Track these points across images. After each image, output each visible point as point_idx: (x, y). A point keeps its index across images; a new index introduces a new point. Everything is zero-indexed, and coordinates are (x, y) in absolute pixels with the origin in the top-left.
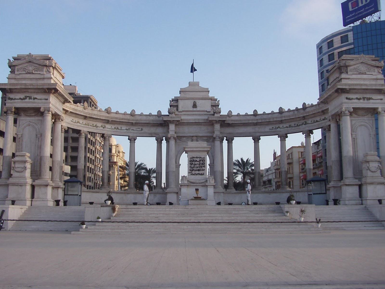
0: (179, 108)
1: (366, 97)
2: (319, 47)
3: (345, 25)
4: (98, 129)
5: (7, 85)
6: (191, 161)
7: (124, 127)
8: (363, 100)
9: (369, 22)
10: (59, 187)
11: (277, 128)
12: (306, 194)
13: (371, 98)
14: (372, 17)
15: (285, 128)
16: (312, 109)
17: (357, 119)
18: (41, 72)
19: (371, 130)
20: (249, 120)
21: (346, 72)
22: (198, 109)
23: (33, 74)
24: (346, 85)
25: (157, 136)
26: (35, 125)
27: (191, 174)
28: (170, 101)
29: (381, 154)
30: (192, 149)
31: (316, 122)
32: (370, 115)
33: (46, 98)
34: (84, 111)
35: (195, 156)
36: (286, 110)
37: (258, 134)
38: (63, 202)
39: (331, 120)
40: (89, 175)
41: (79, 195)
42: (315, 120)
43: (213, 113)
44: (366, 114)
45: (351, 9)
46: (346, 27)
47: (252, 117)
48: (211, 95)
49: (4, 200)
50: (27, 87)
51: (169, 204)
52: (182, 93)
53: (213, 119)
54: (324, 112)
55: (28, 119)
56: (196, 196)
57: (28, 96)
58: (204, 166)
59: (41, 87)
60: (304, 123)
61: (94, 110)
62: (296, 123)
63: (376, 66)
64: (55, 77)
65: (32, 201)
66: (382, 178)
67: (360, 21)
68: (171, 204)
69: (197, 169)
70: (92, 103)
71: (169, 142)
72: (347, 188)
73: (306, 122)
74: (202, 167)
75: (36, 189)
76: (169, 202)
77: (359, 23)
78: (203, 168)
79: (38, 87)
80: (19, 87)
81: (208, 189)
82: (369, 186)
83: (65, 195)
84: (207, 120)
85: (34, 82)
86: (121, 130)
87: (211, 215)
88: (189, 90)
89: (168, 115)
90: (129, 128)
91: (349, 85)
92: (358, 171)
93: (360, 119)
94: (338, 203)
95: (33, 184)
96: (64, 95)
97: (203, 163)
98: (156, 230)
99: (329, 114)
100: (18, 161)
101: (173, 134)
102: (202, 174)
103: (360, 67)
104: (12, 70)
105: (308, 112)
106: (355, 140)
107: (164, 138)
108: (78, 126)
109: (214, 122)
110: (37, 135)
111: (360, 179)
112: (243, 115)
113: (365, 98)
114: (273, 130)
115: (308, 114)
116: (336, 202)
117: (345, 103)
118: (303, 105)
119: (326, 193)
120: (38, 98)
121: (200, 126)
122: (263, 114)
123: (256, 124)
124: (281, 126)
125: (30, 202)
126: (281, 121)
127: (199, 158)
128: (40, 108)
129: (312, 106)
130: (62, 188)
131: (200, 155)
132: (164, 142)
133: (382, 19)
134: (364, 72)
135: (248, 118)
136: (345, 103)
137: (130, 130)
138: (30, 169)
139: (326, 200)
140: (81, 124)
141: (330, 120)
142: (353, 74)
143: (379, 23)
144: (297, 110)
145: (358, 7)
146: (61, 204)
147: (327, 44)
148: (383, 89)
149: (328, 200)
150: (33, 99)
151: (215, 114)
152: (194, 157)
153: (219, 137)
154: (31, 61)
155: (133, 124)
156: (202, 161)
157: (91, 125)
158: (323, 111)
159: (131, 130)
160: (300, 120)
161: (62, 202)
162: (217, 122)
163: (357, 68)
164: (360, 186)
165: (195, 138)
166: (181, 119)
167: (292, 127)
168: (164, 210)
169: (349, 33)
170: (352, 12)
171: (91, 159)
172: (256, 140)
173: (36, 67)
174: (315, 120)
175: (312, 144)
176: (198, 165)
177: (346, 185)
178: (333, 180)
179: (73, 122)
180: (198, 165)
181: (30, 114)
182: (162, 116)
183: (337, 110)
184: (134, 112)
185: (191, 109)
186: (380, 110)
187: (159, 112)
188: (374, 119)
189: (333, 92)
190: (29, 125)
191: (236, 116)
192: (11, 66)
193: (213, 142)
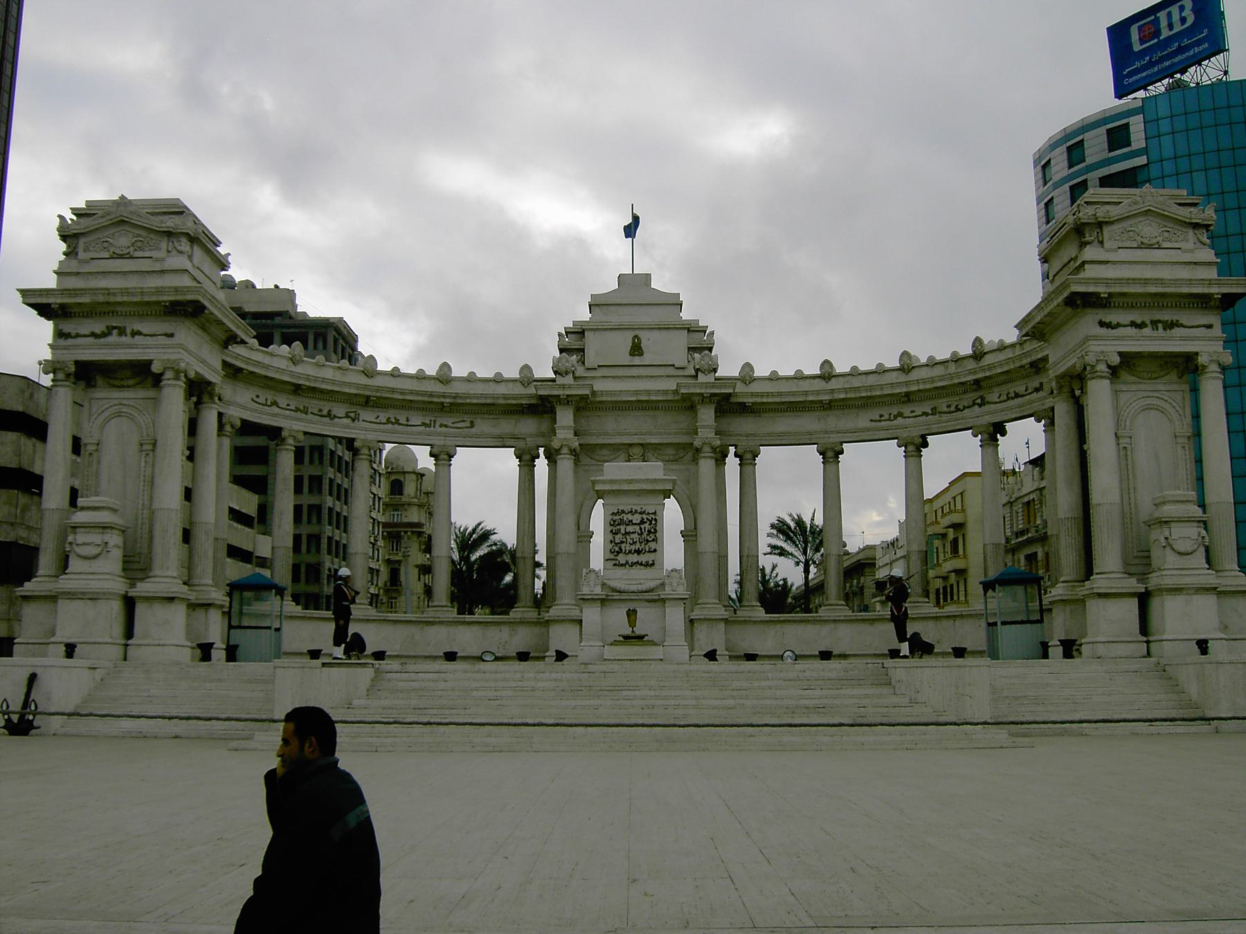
0: (588, 357)
1: (1162, 319)
2: (1040, 162)
3: (1119, 95)
4: (336, 425)
5: (53, 293)
6: (614, 521)
7: (416, 419)
8: (1153, 329)
9: (1192, 85)
10: (210, 605)
11: (896, 417)
12: (983, 624)
13: (1178, 321)
14: (1202, 71)
15: (919, 416)
16: (1002, 356)
17: (1134, 387)
18: (153, 252)
19: (1177, 423)
20: (806, 393)
21: (1099, 241)
22: (647, 359)
23: (132, 257)
24: (1096, 281)
25: (521, 444)
26: (136, 415)
27: (615, 565)
28: (560, 335)
29: (1209, 499)
30: (615, 487)
31: (1013, 398)
32: (1173, 376)
33: (169, 332)
34: (293, 368)
35: (627, 509)
36: (923, 360)
37: (835, 438)
38: (225, 649)
39: (1055, 392)
40: (333, 563)
41: (273, 629)
42: (1012, 391)
43: (693, 373)
44: (1162, 373)
45: (1137, 47)
46: (1122, 102)
47: (820, 385)
48: (686, 315)
49: (42, 641)
50: (112, 299)
51: (715, 655)
52: (596, 309)
53: (692, 391)
54: (1038, 366)
55: (117, 394)
56: (628, 631)
57: (114, 325)
58: (653, 540)
59: (154, 299)
60: (979, 401)
61: (323, 365)
62: (953, 401)
63: (1191, 224)
64: (198, 268)
65: (126, 645)
66: (1210, 571)
67: (1166, 81)
68: (561, 656)
69: (633, 547)
70: (341, 341)
71: (556, 462)
72: (1101, 602)
73: (982, 398)
74: (648, 541)
75: (140, 609)
76: (556, 651)
77: (1163, 89)
78: (653, 545)
79: (146, 299)
80: (86, 299)
81: (667, 609)
82: (1170, 597)
83: (230, 627)
84: (676, 392)
85: (132, 283)
86: (407, 425)
87: (664, 693)
88: (619, 301)
89: (553, 380)
90: (431, 421)
91: (1107, 282)
92: (1138, 552)
93: (1142, 387)
94: (1077, 650)
95: (130, 595)
96: (225, 321)
97: (652, 530)
98: (489, 738)
99: (1050, 372)
100: (85, 523)
101: (569, 440)
102: (647, 565)
103: (1140, 228)
104: (69, 247)
105: (990, 367)
106: (1129, 453)
107: (541, 450)
108: (276, 415)
109: (696, 399)
110: (141, 445)
111: (1143, 577)
112: (787, 378)
113: (1159, 321)
114: (883, 423)
115: (988, 374)
116: (1070, 648)
117: (1095, 338)
118: (973, 346)
119: (1041, 621)
120: (145, 331)
121: (651, 413)
122: (927, 365)
123: (828, 406)
124: (906, 411)
125: (122, 648)
126: (907, 394)
127: (641, 513)
128: (150, 362)
129: (1002, 347)
130: (222, 606)
131: (644, 505)
132: (541, 465)
133: (1234, 76)
134: (1154, 241)
135: (805, 386)
136: (1095, 338)
137: (434, 427)
138: (122, 550)
139: (1041, 643)
140: (283, 408)
141: (1052, 392)
142: (1119, 248)
143: (1222, 87)
144: (955, 361)
145: (1158, 38)
146: (218, 654)
147: (1065, 154)
148: (1212, 294)
149: (1047, 641)
150: (129, 335)
151: (699, 373)
152: (623, 512)
153: (712, 448)
154: (124, 221)
155: (444, 406)
156: (648, 522)
157: (316, 411)
158: (1033, 364)
159: (437, 426)
160: (965, 392)
161: (221, 649)
162: (705, 399)
163: (1131, 229)
164: (1144, 599)
165: (637, 451)
166: (594, 391)
167: (940, 413)
168: (518, 676)
169: (1132, 120)
170: (1143, 53)
171: (338, 513)
172: (831, 455)
173: (139, 236)
174: (1012, 391)
175: (1025, 463)
176: (635, 536)
177: (1100, 595)
178: (1062, 579)
179: (256, 402)
180: (635, 536)
181: (122, 379)
182: (534, 381)
183: (1070, 364)
184: (446, 369)
185: (627, 360)
186: (1202, 360)
187: (526, 368)
188: (1186, 387)
189: (1058, 305)
190: (119, 415)
191: (767, 382)
192: (67, 234)
193: (694, 461)
